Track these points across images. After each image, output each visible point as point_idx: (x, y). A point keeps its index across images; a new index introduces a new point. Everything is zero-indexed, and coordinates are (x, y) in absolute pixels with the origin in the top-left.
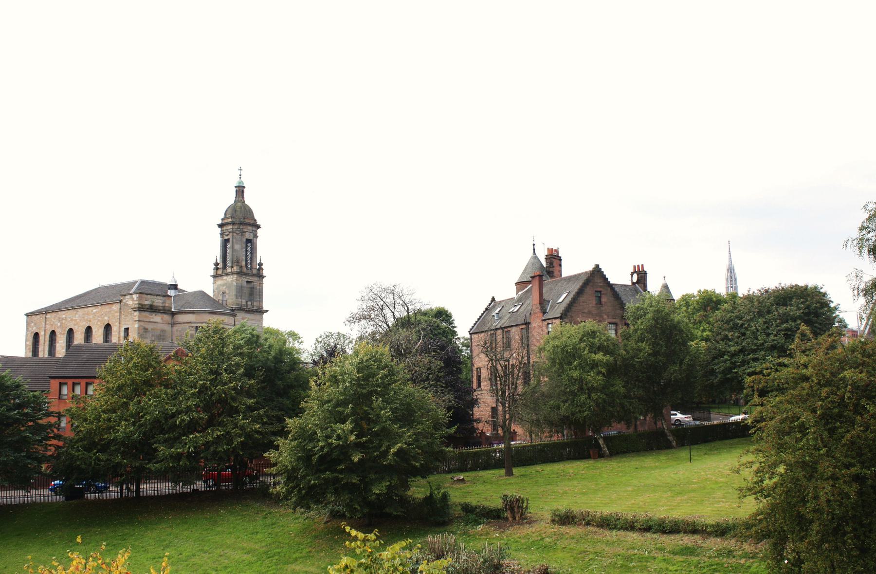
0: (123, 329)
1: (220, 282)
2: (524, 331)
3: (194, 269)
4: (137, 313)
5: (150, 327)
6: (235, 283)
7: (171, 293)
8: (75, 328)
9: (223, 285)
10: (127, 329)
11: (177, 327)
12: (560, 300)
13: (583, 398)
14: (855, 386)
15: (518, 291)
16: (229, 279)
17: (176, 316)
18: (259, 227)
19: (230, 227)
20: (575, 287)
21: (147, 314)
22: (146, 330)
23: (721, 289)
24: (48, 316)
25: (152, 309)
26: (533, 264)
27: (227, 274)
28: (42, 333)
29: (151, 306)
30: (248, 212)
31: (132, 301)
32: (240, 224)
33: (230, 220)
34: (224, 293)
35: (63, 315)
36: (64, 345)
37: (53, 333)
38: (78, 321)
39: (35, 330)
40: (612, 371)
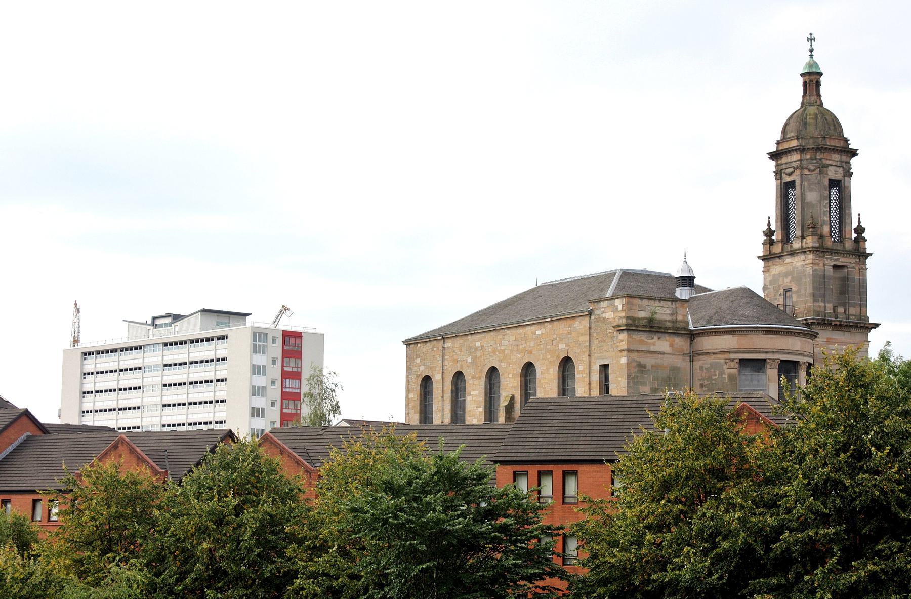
0: (596, 368)
1: (778, 268)
4: (624, 336)
5: (649, 361)
6: (809, 270)
7: (682, 293)
9: (786, 275)
11: (698, 364)
16: (798, 262)
17: (698, 340)
18: (854, 153)
19: (796, 157)
21: (643, 337)
22: (641, 367)
24: (448, 344)
25: (652, 327)
27: (793, 253)
28: (437, 377)
29: (651, 320)
30: (832, 124)
31: (614, 311)
32: (815, 150)
33: (794, 143)
35: (477, 341)
36: (482, 398)
37: (459, 375)
38: (507, 352)
39: (423, 371)
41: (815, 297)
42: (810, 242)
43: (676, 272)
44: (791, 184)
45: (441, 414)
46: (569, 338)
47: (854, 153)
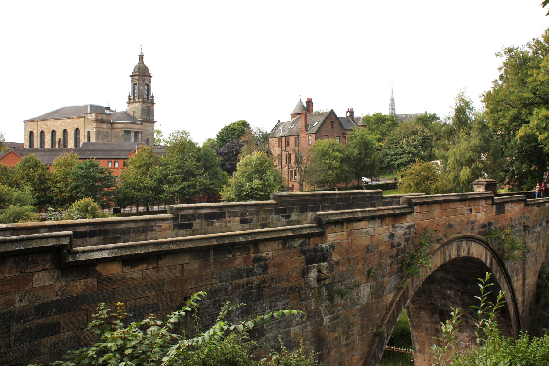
0: (86, 132)
1: (131, 106)
2: (297, 139)
3: (119, 101)
4: (95, 124)
5: (101, 130)
6: (140, 107)
7: (107, 112)
8: (56, 130)
9: (134, 108)
10: (89, 132)
11: (113, 131)
12: (315, 125)
13: (331, 172)
14: (424, 176)
15: (292, 118)
16: (137, 105)
17: (114, 125)
18: (151, 77)
19: (137, 77)
20: (322, 119)
21: (99, 124)
22: (99, 132)
23: (386, 112)
24: (39, 123)
25: (102, 121)
26: (300, 105)
27: (136, 102)
28: (35, 132)
29: (102, 119)
30: (146, 69)
31: (93, 117)
32: (142, 75)
33: (137, 73)
34: (134, 112)
35: (48, 123)
36: (50, 138)
37: (42, 132)
38: (59, 126)
39: (30, 130)
40: (343, 160)
41: (142, 114)
42: (141, 100)
43: (105, 106)
44: (136, 84)
45: (36, 144)
46: (79, 123)
47: (151, 77)
